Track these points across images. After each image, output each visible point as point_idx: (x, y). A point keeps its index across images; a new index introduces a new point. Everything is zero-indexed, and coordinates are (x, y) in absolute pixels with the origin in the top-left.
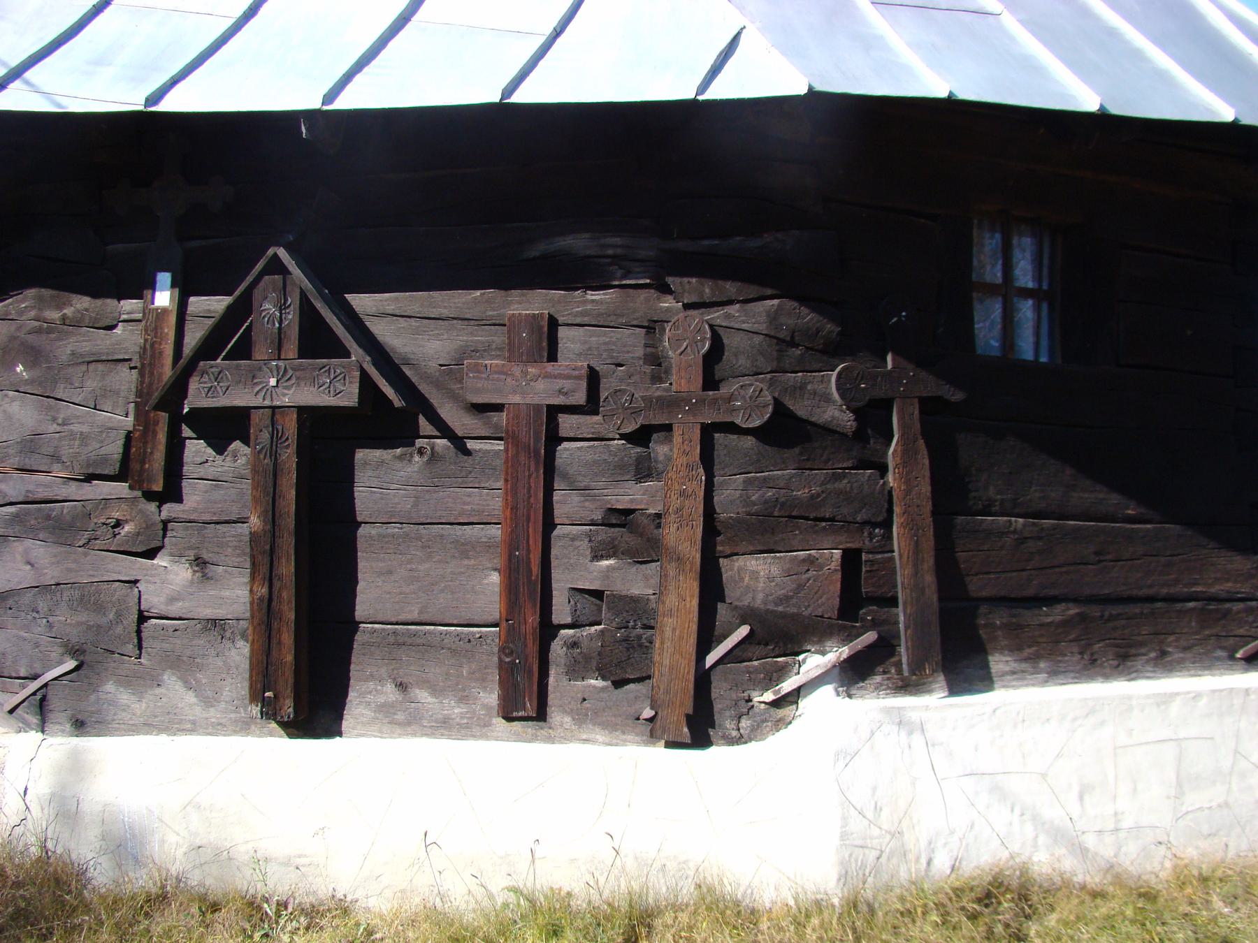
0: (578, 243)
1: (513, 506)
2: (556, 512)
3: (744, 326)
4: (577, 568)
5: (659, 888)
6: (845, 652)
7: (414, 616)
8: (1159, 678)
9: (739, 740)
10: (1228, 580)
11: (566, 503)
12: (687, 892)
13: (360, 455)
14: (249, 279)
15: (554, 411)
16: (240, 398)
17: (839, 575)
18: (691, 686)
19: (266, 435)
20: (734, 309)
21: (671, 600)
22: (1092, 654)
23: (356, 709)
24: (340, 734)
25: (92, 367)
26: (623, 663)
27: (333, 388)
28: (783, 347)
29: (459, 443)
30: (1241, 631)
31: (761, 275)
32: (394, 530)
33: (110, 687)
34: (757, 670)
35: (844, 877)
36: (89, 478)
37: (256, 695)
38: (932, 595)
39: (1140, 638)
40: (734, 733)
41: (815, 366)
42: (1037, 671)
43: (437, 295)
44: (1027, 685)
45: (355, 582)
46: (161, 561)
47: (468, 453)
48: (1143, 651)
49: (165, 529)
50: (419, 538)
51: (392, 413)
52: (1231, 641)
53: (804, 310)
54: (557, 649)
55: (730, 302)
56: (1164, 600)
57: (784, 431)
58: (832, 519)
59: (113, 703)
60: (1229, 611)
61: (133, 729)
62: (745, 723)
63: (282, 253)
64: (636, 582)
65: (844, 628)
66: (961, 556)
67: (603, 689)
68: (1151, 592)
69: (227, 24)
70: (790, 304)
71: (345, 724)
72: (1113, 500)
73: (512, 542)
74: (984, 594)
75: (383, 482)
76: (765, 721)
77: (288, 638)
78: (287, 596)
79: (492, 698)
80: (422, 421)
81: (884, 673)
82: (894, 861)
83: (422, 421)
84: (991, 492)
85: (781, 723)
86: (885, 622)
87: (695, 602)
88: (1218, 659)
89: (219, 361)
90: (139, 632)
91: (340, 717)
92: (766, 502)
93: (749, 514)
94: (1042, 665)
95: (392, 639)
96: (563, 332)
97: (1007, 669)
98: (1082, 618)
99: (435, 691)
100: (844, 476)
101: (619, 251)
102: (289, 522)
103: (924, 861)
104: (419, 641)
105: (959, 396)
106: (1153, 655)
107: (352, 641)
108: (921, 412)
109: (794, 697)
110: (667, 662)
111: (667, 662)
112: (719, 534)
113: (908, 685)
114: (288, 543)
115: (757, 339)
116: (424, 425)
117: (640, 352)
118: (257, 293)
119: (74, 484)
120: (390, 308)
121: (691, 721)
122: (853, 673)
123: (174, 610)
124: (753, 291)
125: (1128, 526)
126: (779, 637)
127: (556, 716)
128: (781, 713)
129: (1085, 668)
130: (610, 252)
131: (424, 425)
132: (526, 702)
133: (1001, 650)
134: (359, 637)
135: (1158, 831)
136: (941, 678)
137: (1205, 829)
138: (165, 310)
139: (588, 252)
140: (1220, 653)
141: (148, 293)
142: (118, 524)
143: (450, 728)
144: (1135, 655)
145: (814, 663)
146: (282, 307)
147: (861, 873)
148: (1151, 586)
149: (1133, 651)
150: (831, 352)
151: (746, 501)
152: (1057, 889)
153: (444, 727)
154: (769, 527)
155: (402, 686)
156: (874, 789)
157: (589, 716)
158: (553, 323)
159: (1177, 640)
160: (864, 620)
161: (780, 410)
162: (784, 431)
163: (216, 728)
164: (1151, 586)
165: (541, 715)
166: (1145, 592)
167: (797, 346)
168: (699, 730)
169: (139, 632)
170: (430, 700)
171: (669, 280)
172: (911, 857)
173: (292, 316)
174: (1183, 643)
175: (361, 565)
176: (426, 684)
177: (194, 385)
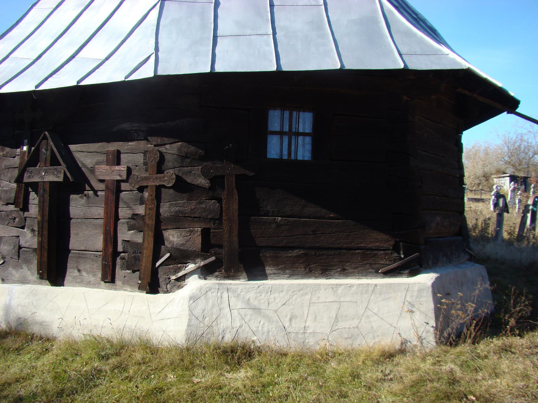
0: (126, 126)
1: (106, 213)
2: (120, 215)
3: (171, 152)
4: (125, 234)
5: (127, 336)
6: (202, 263)
7: (83, 248)
8: (341, 279)
9: (167, 292)
10: (377, 242)
11: (124, 212)
12: (136, 340)
13: (72, 197)
14: (39, 141)
15: (119, 182)
16: (36, 179)
17: (200, 237)
18: (150, 273)
19: (42, 191)
20: (168, 146)
21: (146, 244)
22: (310, 269)
23: (68, 278)
24: (63, 285)
25: (10, 169)
26: (132, 265)
27: (54, 176)
28: (183, 158)
29: (96, 192)
30: (382, 262)
31: (175, 135)
32: (79, 220)
33: (10, 269)
34: (171, 268)
35: (188, 339)
36: (8, 204)
37: (38, 273)
38: (236, 245)
39: (333, 263)
40: (165, 289)
41: (196, 165)
42: (285, 273)
43: (91, 145)
44: (280, 279)
45: (70, 237)
46: (25, 230)
47: (97, 196)
48: (335, 268)
49: (25, 220)
50: (85, 223)
51: (78, 181)
52: (377, 266)
53: (190, 146)
54: (118, 260)
55: (166, 144)
56: (345, 249)
57: (181, 186)
58: (200, 217)
59: (11, 274)
60: (377, 254)
61: (14, 282)
62: (169, 286)
63: (46, 133)
64: (138, 238)
65: (202, 256)
66: (252, 231)
67: (130, 273)
68: (339, 246)
69: (30, 62)
70: (185, 144)
71: (65, 282)
72: (324, 212)
73: (106, 225)
74: (262, 245)
75: (77, 206)
76: (175, 286)
77: (46, 254)
78: (46, 240)
79: (100, 275)
80: (87, 186)
81: (219, 271)
82: (209, 336)
83: (87, 186)
84: (269, 208)
85: (180, 287)
86: (219, 254)
87: (152, 245)
88: (370, 272)
89: (38, 167)
90: (19, 252)
91: (64, 280)
92: (176, 212)
93: (171, 215)
94: (287, 272)
95: (78, 255)
96: (122, 156)
97: (272, 272)
98: (306, 255)
99: (88, 273)
100: (204, 202)
101: (137, 128)
102: (46, 218)
103: (220, 337)
104: (85, 256)
105: (252, 174)
106: (339, 270)
107: (68, 256)
108: (236, 179)
109: (183, 278)
110: (144, 265)
111: (144, 265)
112: (162, 222)
113: (229, 276)
114: (46, 225)
115: (175, 156)
116: (87, 188)
117: (142, 161)
118: (41, 146)
119: (4, 206)
120: (79, 149)
121: (150, 285)
122: (206, 272)
123: (26, 245)
124: (172, 140)
125: (330, 221)
126: (180, 257)
127: (118, 282)
128: (179, 283)
129: (307, 273)
130: (134, 129)
131: (87, 188)
132: (109, 277)
133: (270, 265)
134: (70, 255)
135: (323, 335)
136: (244, 274)
137: (346, 336)
138: (25, 151)
139: (129, 129)
140: (371, 270)
141: (22, 147)
142: (15, 218)
143: (90, 285)
144: (331, 270)
145: (191, 267)
146: (47, 150)
147: (195, 339)
148: (339, 244)
149: (330, 268)
150: (202, 159)
151: (170, 212)
152: (190, 320)
153: (89, 284)
154: (178, 221)
155: (79, 271)
156: (204, 311)
157: (127, 282)
158: (119, 153)
159: (351, 265)
160: (211, 253)
161: (179, 179)
162: (181, 186)
163: (35, 283)
164: (339, 244)
165: (113, 281)
166: (336, 246)
167: (189, 158)
168: (153, 286)
169: (19, 252)
170: (86, 275)
171: (148, 138)
172: (215, 335)
173: (49, 153)
174: (353, 266)
175: (71, 231)
176: (86, 270)
177: (26, 175)
